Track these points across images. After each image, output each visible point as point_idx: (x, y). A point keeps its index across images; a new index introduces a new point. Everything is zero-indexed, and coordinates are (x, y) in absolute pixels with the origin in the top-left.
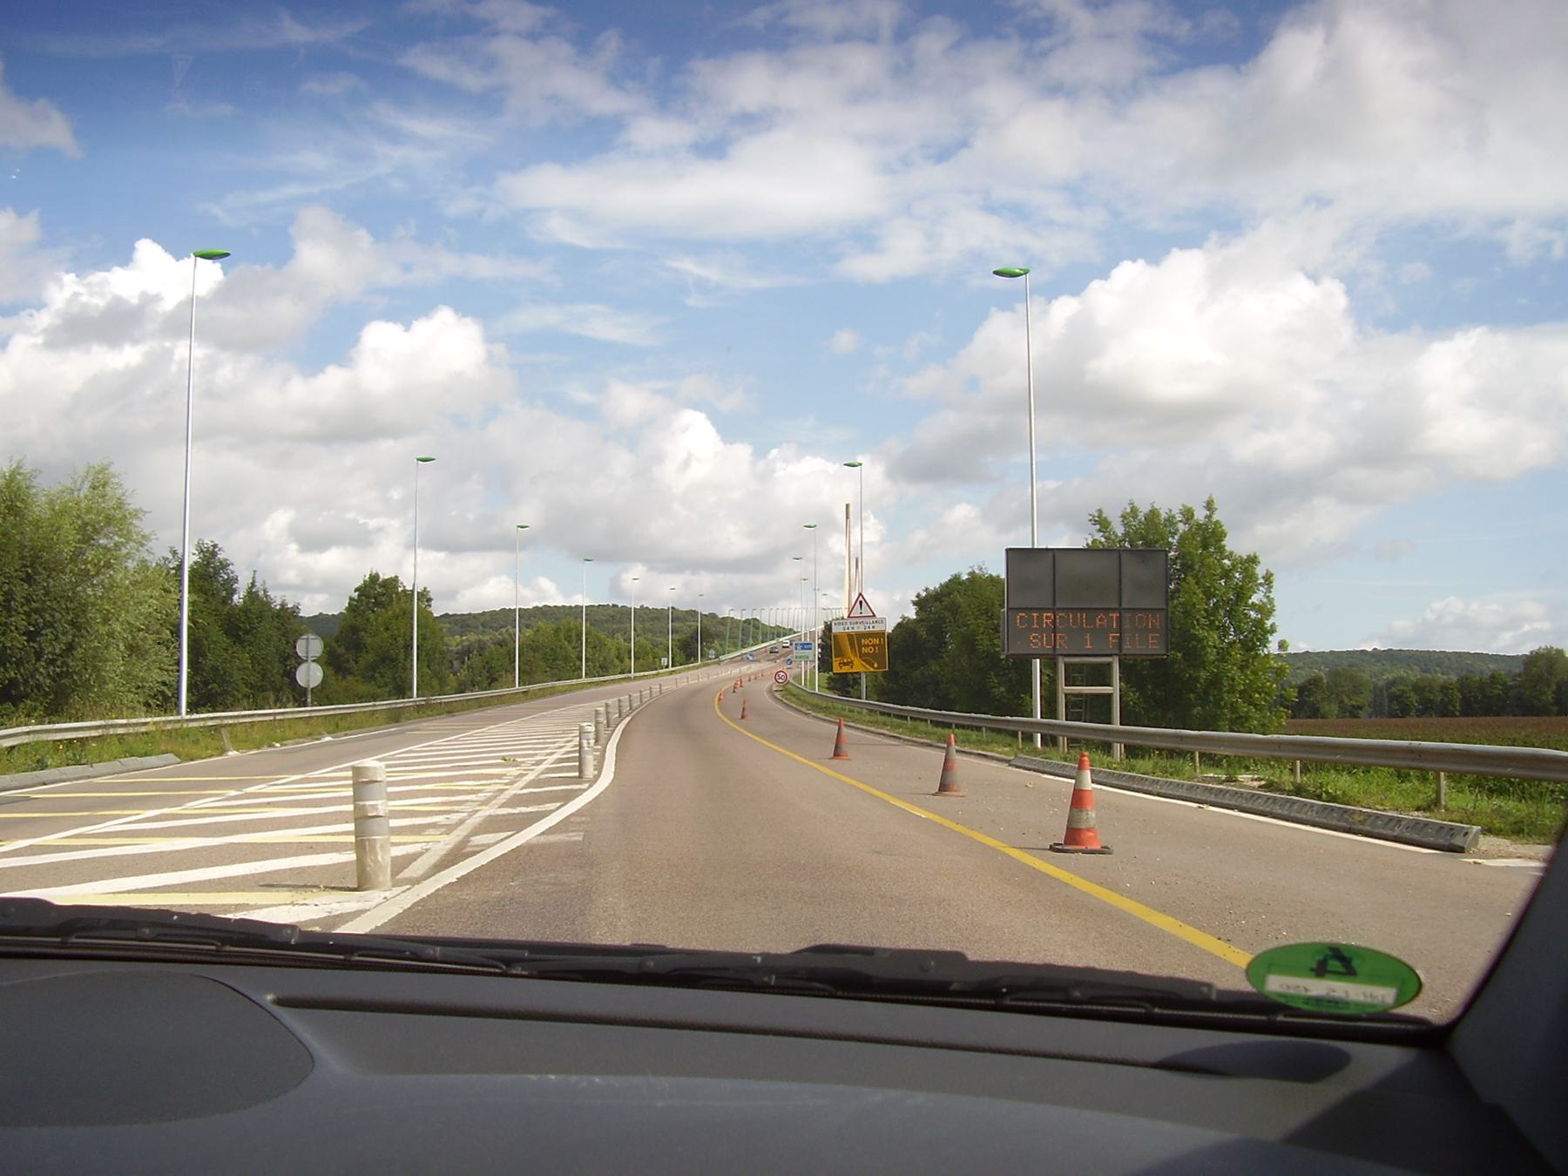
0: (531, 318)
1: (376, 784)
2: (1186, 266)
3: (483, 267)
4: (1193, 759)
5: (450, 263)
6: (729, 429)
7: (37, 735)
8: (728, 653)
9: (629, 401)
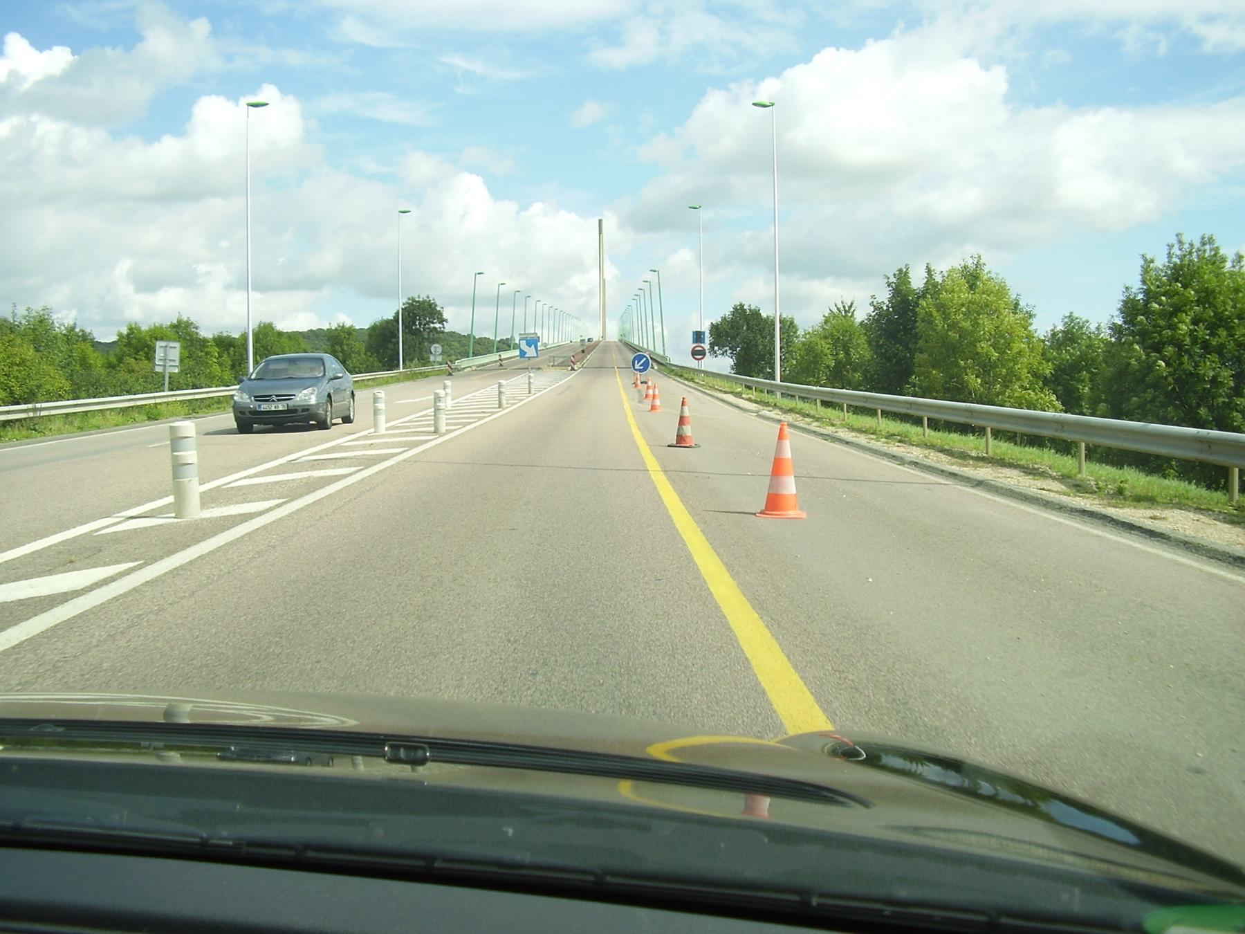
0: (335, 103)
1: (188, 466)
2: (877, 52)
3: (294, 58)
4: (816, 404)
5: (265, 54)
6: (498, 189)
7: (1120, 869)
8: (475, 354)
9: (420, 166)
